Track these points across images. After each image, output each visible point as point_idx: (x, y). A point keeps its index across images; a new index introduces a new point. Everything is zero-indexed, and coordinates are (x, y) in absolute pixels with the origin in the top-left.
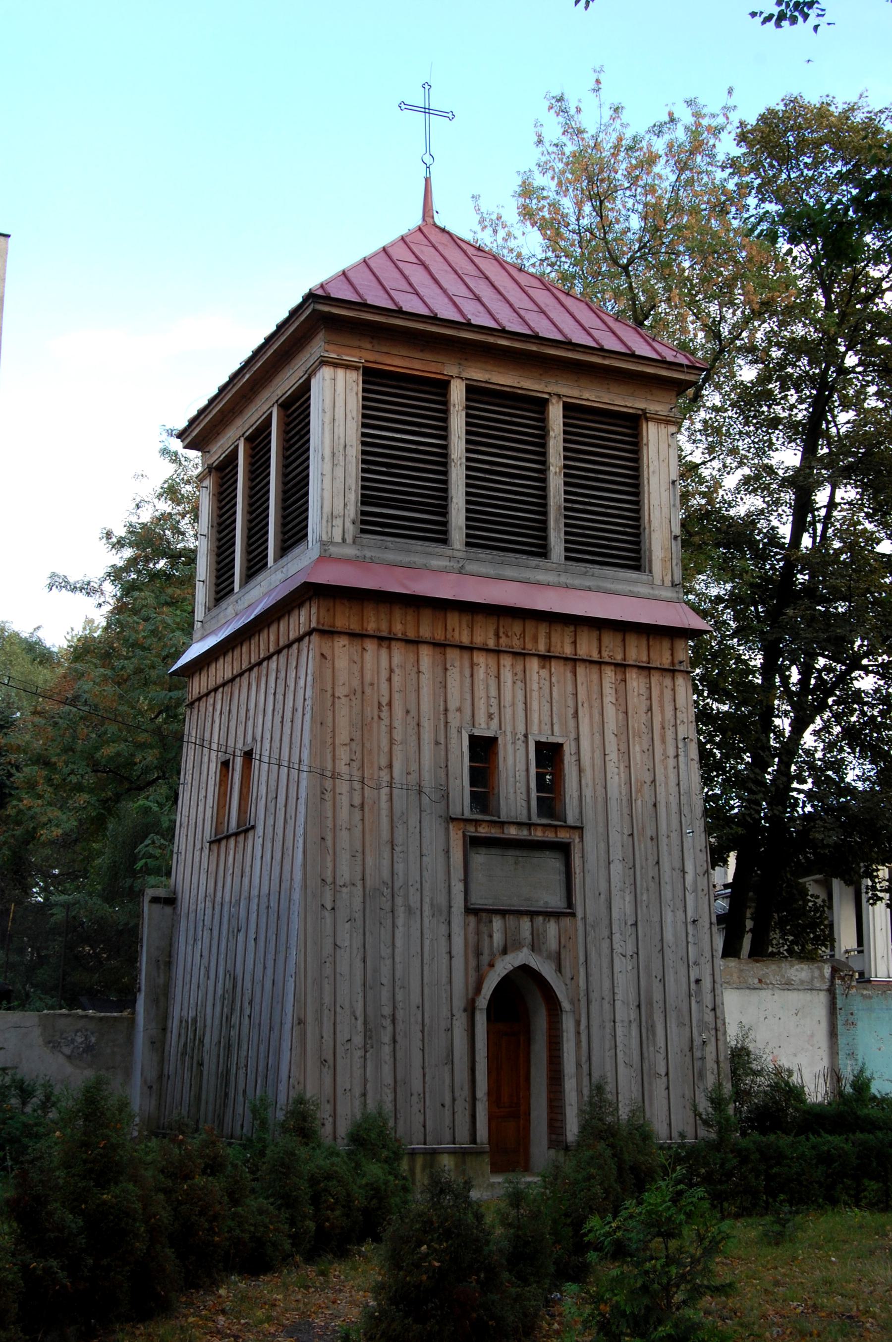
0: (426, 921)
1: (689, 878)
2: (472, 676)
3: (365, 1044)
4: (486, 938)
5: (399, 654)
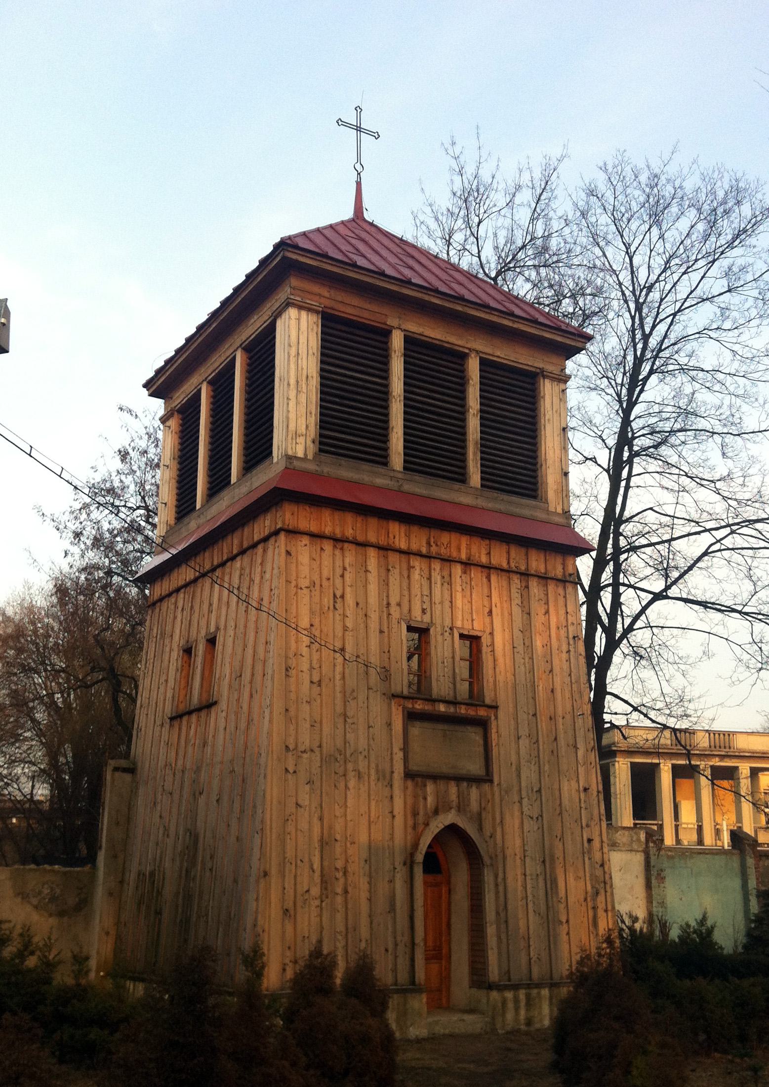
0: (372, 783)
1: (580, 753)
2: (409, 577)
3: (322, 894)
4: (421, 799)
5: (350, 556)
